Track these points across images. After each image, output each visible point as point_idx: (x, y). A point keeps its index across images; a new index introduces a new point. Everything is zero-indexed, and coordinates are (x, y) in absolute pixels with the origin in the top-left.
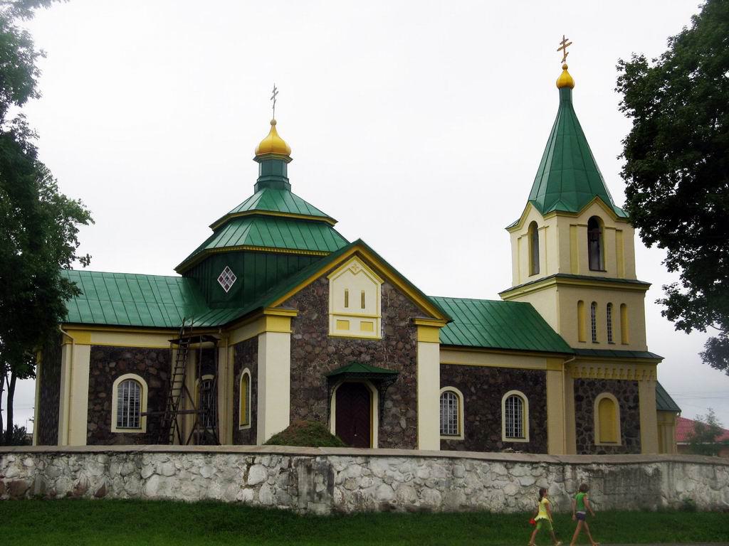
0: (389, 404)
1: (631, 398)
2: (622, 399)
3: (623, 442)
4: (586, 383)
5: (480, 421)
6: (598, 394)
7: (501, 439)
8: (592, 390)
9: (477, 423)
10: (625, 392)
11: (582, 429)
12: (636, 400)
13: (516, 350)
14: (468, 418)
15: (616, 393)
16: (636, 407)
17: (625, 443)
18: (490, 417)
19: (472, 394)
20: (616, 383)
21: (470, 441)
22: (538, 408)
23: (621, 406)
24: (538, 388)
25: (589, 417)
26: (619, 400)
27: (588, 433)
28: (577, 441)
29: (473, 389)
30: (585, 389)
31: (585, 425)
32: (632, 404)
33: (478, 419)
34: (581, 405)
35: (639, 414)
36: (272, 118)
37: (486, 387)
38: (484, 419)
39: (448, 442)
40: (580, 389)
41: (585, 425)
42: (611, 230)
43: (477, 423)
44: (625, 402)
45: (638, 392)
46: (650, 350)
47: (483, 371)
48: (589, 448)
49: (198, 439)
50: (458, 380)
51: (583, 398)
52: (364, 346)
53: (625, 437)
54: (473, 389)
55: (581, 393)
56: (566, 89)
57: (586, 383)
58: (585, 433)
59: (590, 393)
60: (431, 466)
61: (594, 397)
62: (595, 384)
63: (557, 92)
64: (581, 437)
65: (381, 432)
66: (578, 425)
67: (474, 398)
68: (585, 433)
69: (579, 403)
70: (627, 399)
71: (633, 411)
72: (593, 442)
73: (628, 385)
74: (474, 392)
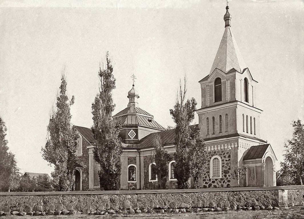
1: (227, 156)
3: (223, 177)
32: (227, 159)
48: (208, 180)
49: (207, 176)
72: (209, 177)
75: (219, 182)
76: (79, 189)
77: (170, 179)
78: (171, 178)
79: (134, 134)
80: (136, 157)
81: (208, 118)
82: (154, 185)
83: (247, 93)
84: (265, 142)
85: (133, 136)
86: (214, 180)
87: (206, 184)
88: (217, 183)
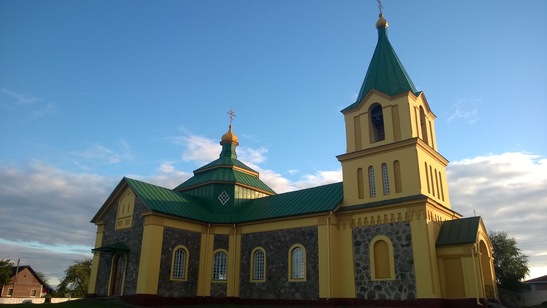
0: (130, 264)
1: (404, 237)
2: (395, 239)
3: (397, 277)
4: (363, 230)
5: (275, 268)
6: (373, 237)
7: (287, 280)
8: (368, 235)
9: (273, 270)
10: (397, 233)
11: (360, 268)
12: (409, 238)
13: (190, 219)
14: (268, 267)
15: (389, 234)
16: (409, 244)
17: (400, 278)
18: (281, 265)
19: (271, 250)
20: (389, 226)
21: (269, 282)
22: (313, 255)
23: (394, 245)
24: (313, 240)
25: (366, 257)
26: (392, 240)
27: (366, 270)
28: (356, 279)
29: (272, 247)
30: (362, 235)
31: (363, 264)
32: (404, 243)
33: (274, 267)
34: (359, 248)
35: (412, 250)
36: (226, 131)
37: (279, 244)
38: (278, 266)
39: (257, 284)
40: (358, 236)
41: (363, 264)
42: (385, 106)
43: (273, 270)
44: (397, 241)
45: (410, 231)
46: (278, 193)
47: (278, 234)
48: (367, 283)
49: (365, 276)
50: (263, 242)
51: (361, 243)
52: (125, 233)
53: (399, 272)
54: (272, 247)
55: (359, 239)
56: (381, 28)
57: (363, 230)
58: (363, 271)
59: (366, 238)
60: (269, 297)
61: (370, 240)
62: (370, 230)
63: (376, 31)
64: (360, 274)
65: (125, 281)
66: (357, 265)
67: (272, 252)
68: (363, 271)
69: (358, 247)
70: (399, 239)
71: (406, 248)
72: (370, 278)
73: (400, 226)
74: (272, 249)
75: (391, 287)
76: (177, 276)
77: (252, 280)
78: (253, 279)
79: (227, 198)
80: (228, 235)
81: (25, 277)
82: (88, 296)
83: (31, 269)
84: (461, 216)
85: (226, 200)
86: (379, 284)
87: (363, 292)
88: (386, 290)
